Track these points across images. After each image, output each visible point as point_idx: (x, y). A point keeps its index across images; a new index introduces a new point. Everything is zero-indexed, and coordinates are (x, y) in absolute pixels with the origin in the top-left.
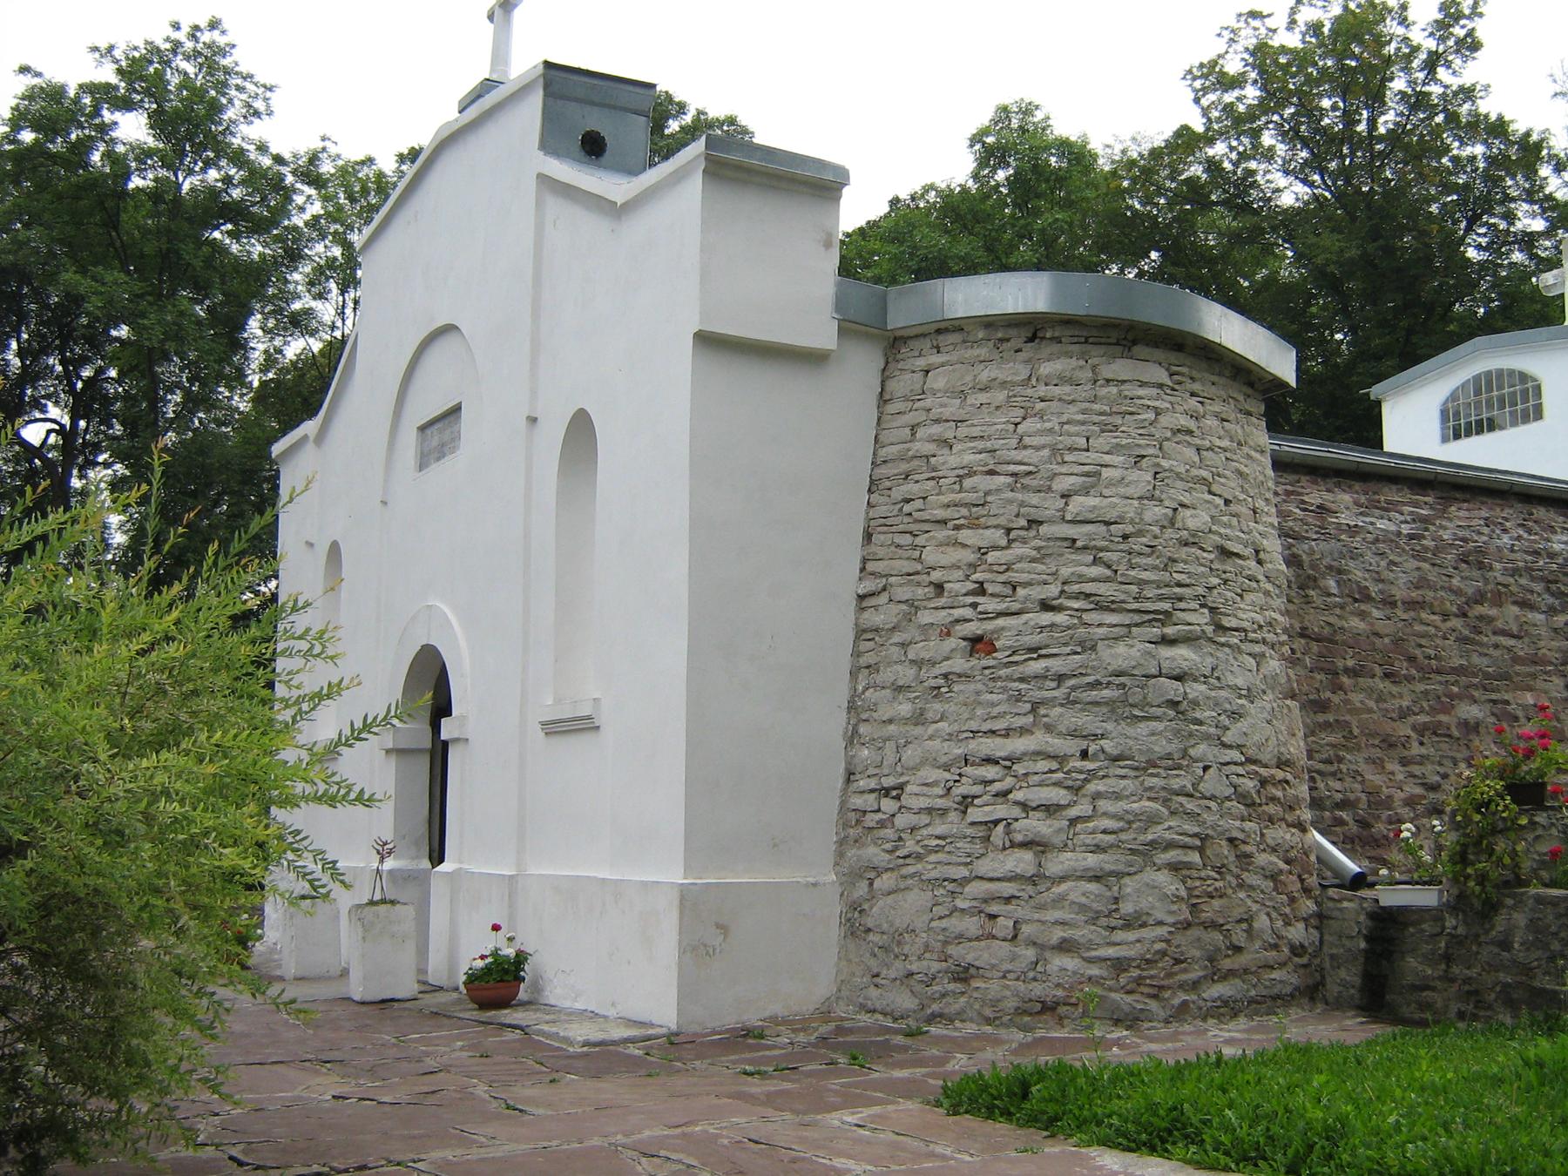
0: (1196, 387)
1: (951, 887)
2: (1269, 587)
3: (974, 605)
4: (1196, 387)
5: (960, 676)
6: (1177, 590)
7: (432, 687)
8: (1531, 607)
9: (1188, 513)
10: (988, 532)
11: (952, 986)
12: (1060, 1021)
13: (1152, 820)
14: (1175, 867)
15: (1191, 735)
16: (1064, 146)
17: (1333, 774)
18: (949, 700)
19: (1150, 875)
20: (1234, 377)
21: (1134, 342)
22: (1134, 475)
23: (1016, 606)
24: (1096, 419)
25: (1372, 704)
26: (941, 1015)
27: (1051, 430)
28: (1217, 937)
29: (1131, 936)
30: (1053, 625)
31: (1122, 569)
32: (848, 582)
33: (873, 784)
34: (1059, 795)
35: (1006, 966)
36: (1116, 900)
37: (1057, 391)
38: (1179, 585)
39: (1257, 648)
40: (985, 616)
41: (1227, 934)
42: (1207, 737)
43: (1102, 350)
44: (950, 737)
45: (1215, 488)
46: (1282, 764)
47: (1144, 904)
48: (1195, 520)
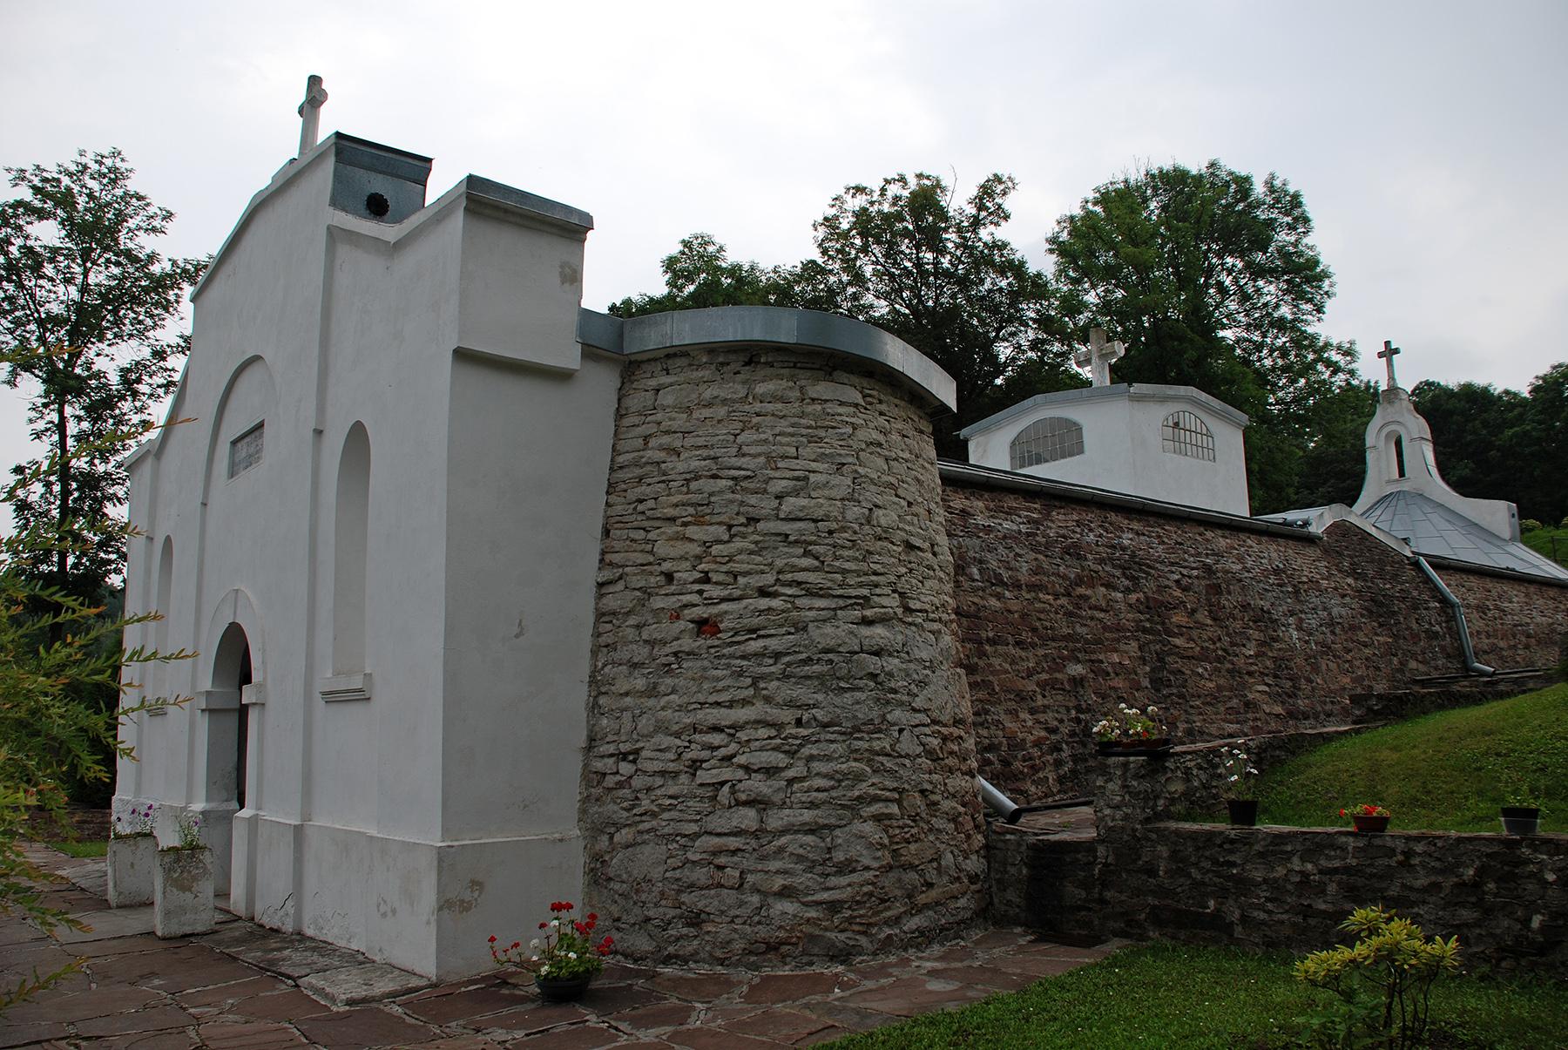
0: (883, 407)
1: (683, 841)
2: (942, 575)
3: (700, 592)
4: (883, 407)
5: (688, 654)
6: (874, 578)
7: (235, 657)
8: (1115, 589)
9: (881, 512)
10: (712, 529)
11: (685, 931)
12: (783, 959)
13: (859, 778)
14: (878, 818)
15: (888, 702)
16: (734, 271)
17: (982, 724)
18: (678, 676)
19: (858, 826)
20: (911, 402)
21: (834, 369)
22: (836, 480)
23: (737, 593)
24: (804, 431)
25: (1007, 666)
26: (677, 957)
27: (766, 441)
28: (913, 875)
29: (844, 881)
30: (769, 609)
31: (828, 560)
32: (590, 572)
33: (612, 749)
34: (779, 759)
35: (733, 913)
36: (829, 850)
37: (770, 407)
38: (875, 573)
39: (936, 626)
40: (710, 602)
41: (922, 873)
42: (902, 704)
43: (809, 374)
44: (680, 708)
45: (900, 492)
46: (957, 722)
47: (853, 853)
48: (885, 518)
